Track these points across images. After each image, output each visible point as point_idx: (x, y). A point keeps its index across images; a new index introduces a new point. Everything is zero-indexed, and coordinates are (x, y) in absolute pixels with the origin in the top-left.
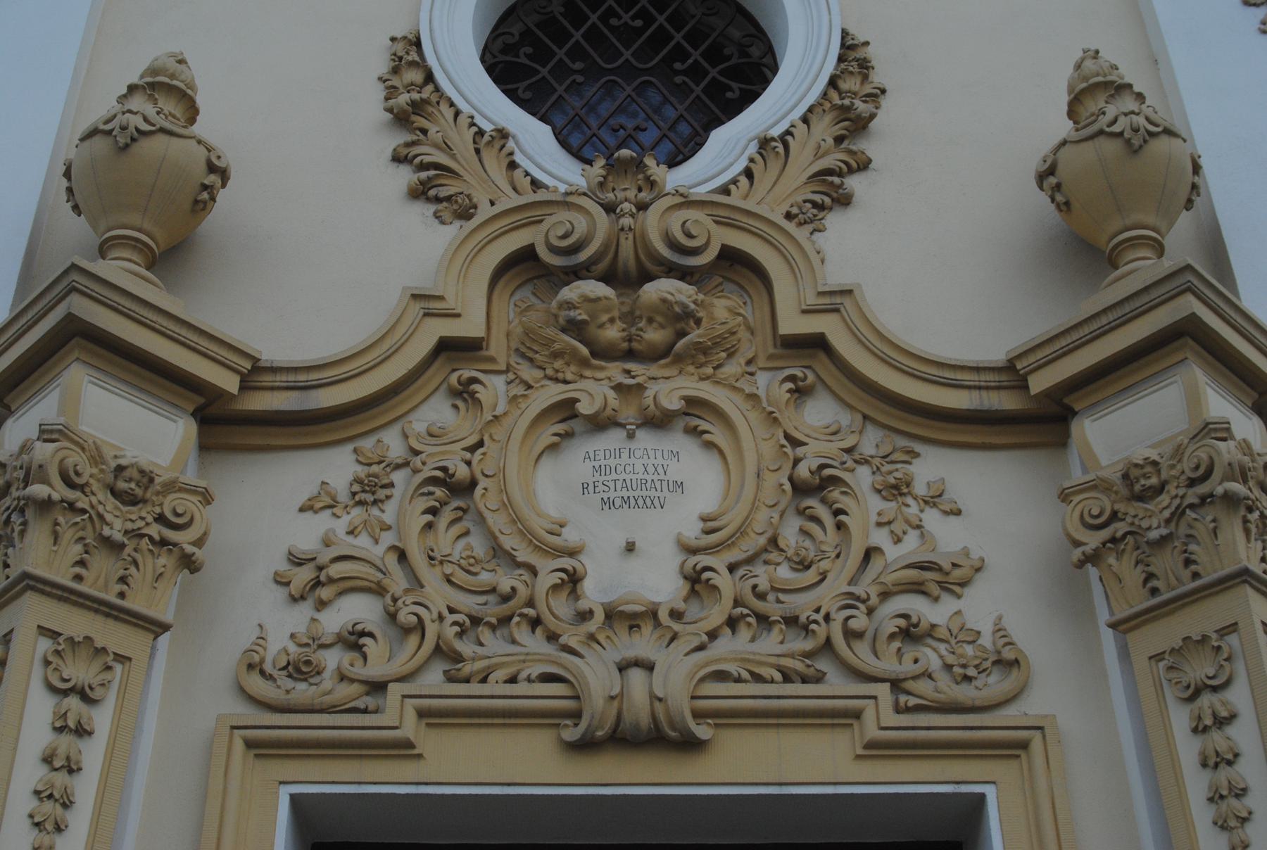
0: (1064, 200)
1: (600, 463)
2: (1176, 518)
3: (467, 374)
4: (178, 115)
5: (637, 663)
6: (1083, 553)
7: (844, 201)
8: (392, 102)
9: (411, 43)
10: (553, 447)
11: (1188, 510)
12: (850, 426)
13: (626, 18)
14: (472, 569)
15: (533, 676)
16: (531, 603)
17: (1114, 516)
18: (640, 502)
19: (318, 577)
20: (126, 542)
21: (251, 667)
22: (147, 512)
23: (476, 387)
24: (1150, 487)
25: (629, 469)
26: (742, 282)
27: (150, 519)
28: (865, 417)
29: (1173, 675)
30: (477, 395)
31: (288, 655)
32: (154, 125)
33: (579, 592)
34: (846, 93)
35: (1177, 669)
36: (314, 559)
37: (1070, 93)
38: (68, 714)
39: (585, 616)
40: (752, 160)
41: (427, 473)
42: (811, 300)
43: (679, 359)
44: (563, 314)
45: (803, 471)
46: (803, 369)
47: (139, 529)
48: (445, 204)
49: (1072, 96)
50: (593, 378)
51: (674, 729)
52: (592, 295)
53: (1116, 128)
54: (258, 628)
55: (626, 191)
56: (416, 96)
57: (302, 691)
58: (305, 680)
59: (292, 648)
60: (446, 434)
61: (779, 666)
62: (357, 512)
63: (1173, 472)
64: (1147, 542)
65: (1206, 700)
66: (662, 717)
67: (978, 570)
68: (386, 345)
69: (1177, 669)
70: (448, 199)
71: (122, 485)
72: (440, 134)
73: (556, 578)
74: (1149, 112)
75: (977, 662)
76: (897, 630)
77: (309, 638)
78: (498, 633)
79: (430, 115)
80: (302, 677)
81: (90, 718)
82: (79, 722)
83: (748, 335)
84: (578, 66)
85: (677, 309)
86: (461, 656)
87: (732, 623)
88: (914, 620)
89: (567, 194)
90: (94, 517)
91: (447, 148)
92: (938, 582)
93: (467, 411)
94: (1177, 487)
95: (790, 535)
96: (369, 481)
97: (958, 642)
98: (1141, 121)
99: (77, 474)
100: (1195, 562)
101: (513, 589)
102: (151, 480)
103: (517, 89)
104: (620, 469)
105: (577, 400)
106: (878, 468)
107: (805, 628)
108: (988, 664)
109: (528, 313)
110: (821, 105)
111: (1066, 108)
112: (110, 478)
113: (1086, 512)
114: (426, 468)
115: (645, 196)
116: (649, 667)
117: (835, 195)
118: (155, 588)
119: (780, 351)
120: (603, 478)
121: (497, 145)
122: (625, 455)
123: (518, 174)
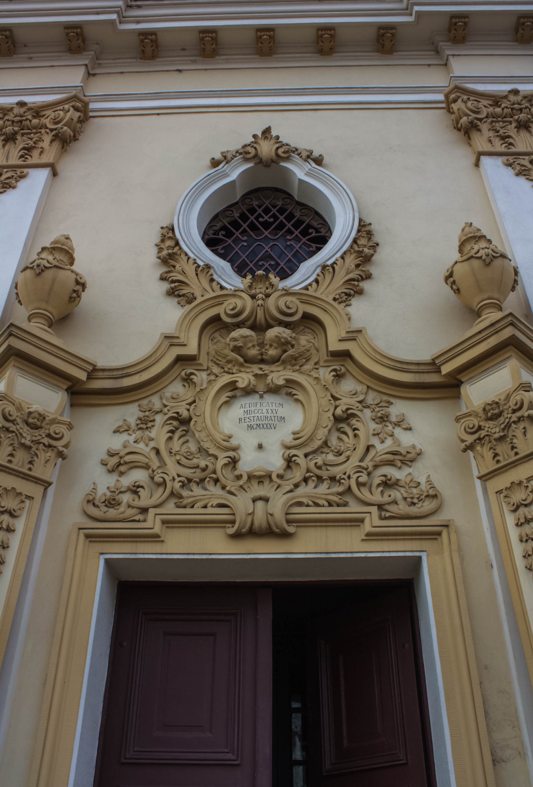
0: (456, 288)
1: (247, 409)
2: (507, 427)
3: (189, 371)
4: (65, 261)
5: (260, 498)
6: (466, 445)
7: (360, 292)
8: (160, 254)
9: (170, 229)
10: (226, 402)
11: (512, 424)
12: (361, 391)
13: (266, 218)
14: (189, 457)
15: (214, 505)
16: (214, 472)
17: (480, 428)
18: (265, 426)
19: (120, 461)
20: (32, 445)
21: (88, 501)
22: (42, 432)
23: (193, 377)
24: (495, 414)
25: (260, 411)
26: (313, 328)
27: (44, 436)
28: (368, 387)
29: (506, 500)
30: (193, 380)
31: (106, 496)
32: (51, 264)
33: (237, 467)
34: (361, 245)
35: (509, 497)
36: (118, 454)
37: (459, 241)
38: (3, 522)
39: (239, 477)
40: (318, 275)
41: (170, 414)
42: (344, 335)
43: (284, 362)
44: (232, 344)
45: (339, 411)
46: (340, 366)
47: (39, 440)
48: (182, 298)
49: (460, 243)
50: (245, 372)
51: (278, 529)
52: (245, 335)
53: (479, 255)
54: (93, 485)
55: (260, 289)
56: (170, 251)
57: (112, 513)
58: (113, 507)
59: (108, 494)
60: (179, 398)
61: (327, 499)
62: (138, 432)
63: (505, 407)
64: (494, 439)
65: (522, 510)
66: (272, 523)
67: (419, 454)
68: (153, 359)
69: (509, 497)
70: (183, 295)
71: (31, 420)
72: (181, 268)
73: (226, 461)
74: (494, 248)
75: (417, 496)
76: (381, 482)
77: (115, 488)
78: (200, 486)
79: (176, 259)
80: (111, 506)
81: (14, 524)
82: (8, 525)
83: (315, 351)
84: (245, 238)
85: (283, 340)
86: (182, 496)
87: (306, 480)
88: (389, 477)
89: (235, 291)
90: (18, 434)
91: (184, 273)
92: (400, 460)
93: (189, 387)
94: (508, 413)
95: (334, 442)
96: (145, 419)
97: (409, 487)
98: (490, 251)
99: (10, 415)
100: (516, 448)
101: (207, 466)
102: (44, 418)
103: (218, 249)
104: (256, 411)
105: (237, 381)
106: (374, 410)
107: (339, 481)
108: (423, 497)
109: (217, 344)
110: (350, 251)
111: (458, 249)
112: (26, 418)
113: (467, 427)
114: (170, 413)
115: (269, 291)
116: (266, 500)
117: (355, 289)
118: (45, 466)
119: (330, 358)
120: (248, 416)
121: (206, 271)
122: (258, 405)
123: (214, 284)
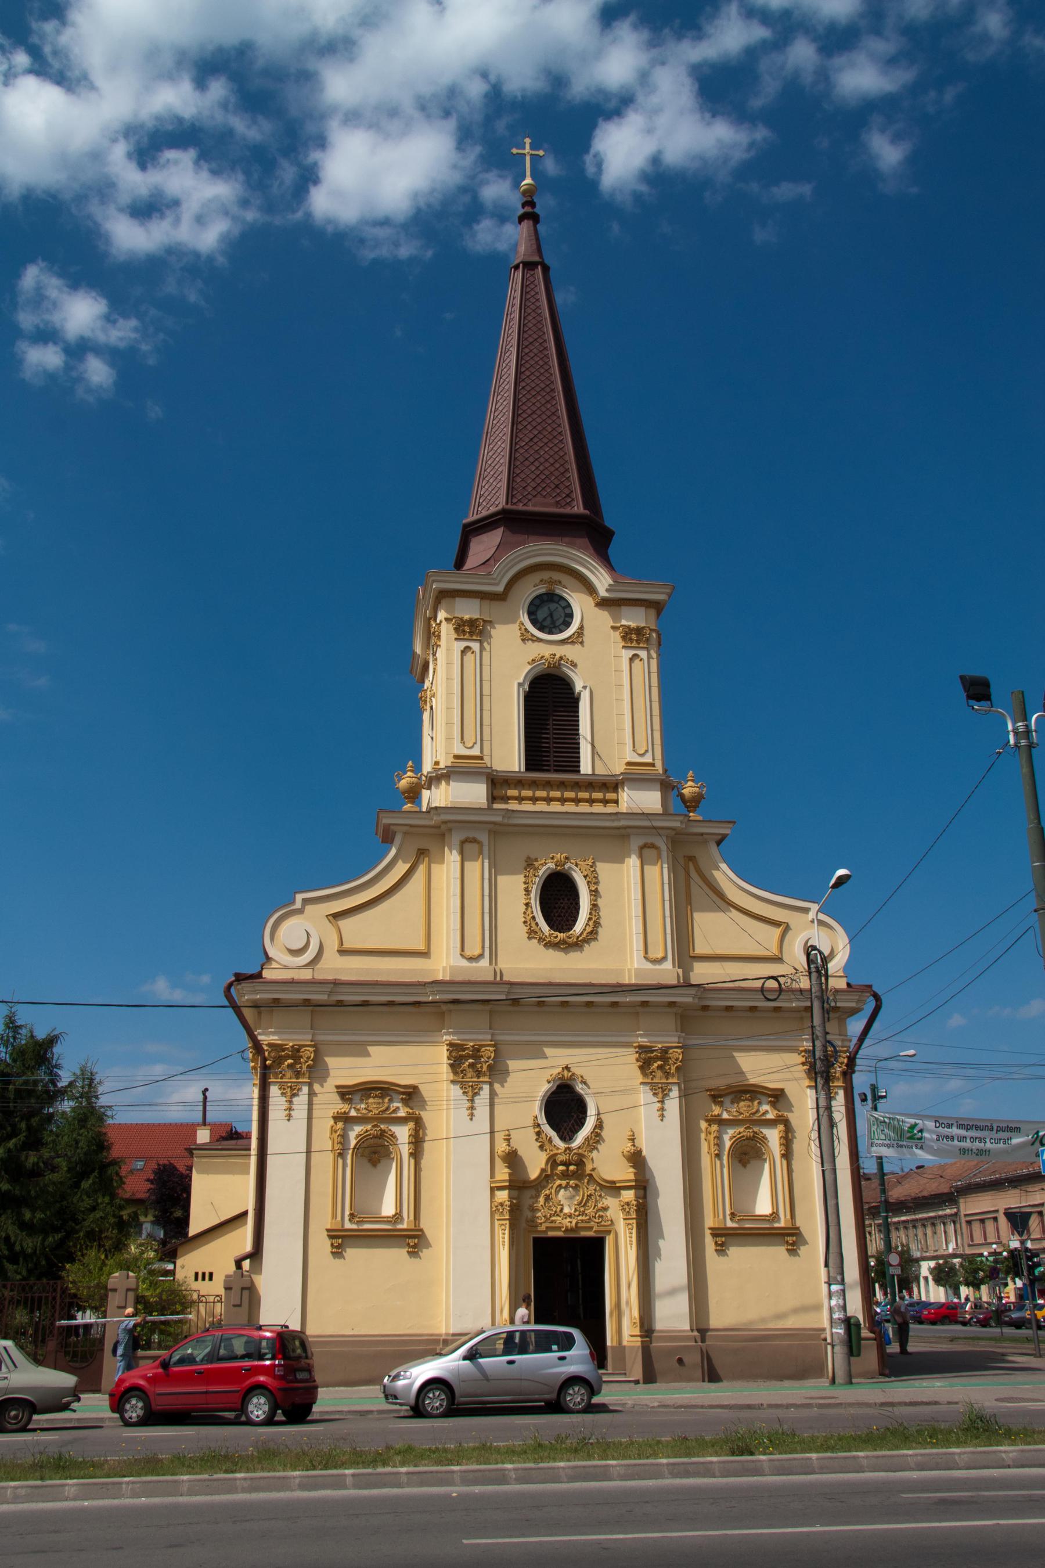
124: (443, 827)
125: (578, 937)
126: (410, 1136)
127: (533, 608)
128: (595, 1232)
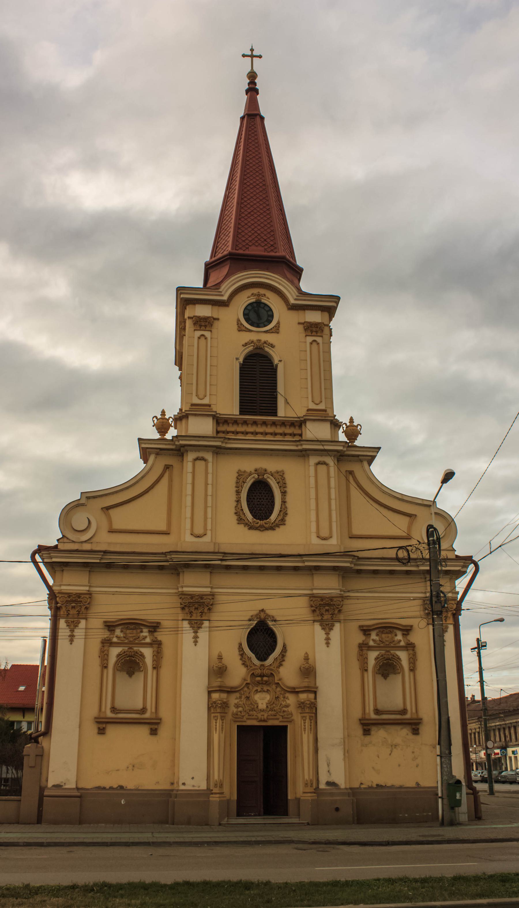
87: (270, 710)
124: (182, 449)
125: (272, 523)
126: (153, 656)
127: (247, 312)
128: (280, 722)
